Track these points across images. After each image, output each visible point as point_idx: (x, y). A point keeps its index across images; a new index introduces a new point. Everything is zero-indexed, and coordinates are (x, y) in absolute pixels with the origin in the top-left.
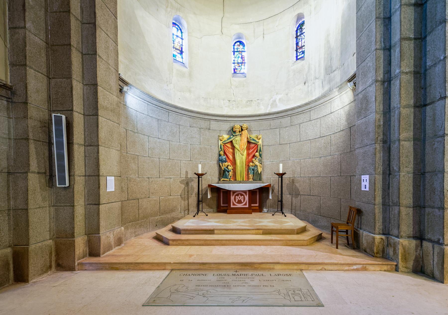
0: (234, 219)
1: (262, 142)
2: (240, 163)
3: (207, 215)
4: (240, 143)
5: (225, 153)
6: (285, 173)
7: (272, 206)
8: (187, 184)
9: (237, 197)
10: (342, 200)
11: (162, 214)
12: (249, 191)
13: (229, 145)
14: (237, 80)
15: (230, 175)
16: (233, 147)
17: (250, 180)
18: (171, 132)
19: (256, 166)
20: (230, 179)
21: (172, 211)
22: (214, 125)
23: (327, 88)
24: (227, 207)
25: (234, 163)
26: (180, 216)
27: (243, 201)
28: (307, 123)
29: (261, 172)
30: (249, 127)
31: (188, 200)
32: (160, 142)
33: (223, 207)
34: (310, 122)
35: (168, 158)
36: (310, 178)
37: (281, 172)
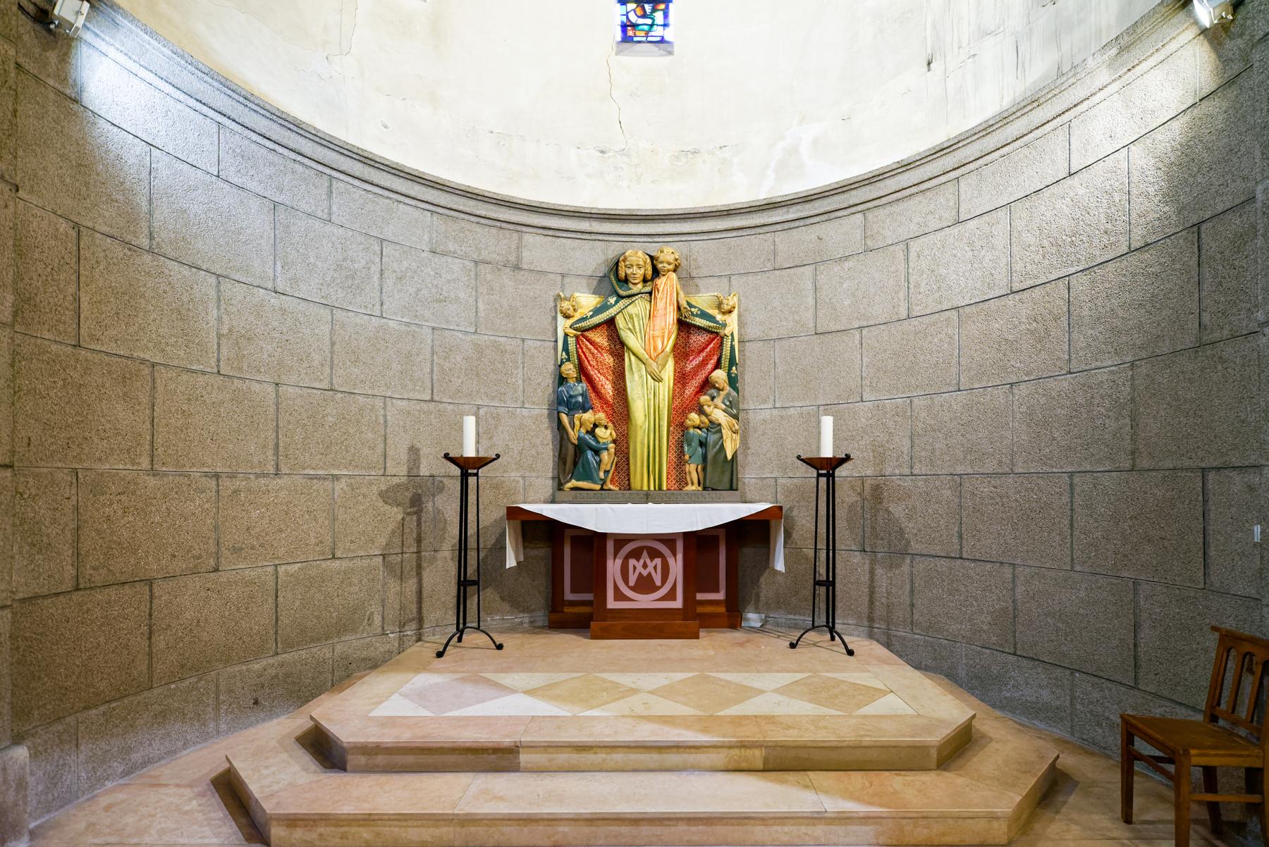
0: (624, 670)
1: (741, 324)
2: (647, 416)
3: (500, 647)
4: (649, 327)
5: (582, 369)
6: (847, 458)
7: (781, 603)
8: (416, 504)
9: (632, 562)
10: (1145, 589)
11: (290, 645)
12: (687, 536)
13: (600, 338)
14: (642, 60)
15: (603, 467)
16: (619, 347)
17: (690, 488)
18: (339, 267)
19: (715, 427)
20: (604, 482)
21: (343, 627)
22: (537, 250)
23: (1039, 69)
24: (589, 603)
25: (621, 412)
26: (381, 647)
27: (658, 583)
28: (940, 235)
29: (735, 456)
30: (684, 263)
31: (419, 575)
32: (283, 311)
33: (572, 604)
34: (960, 227)
35: (325, 385)
36: (958, 480)
37: (827, 452)
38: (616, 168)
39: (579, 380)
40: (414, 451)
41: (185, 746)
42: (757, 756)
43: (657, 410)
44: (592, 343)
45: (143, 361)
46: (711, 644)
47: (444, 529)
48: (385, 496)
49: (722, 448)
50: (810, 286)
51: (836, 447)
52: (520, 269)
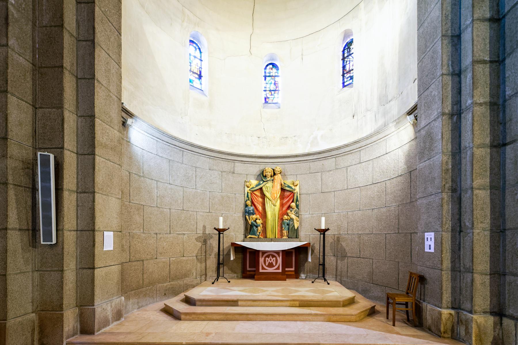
1: (300, 189)
2: (272, 216)
3: (229, 282)
4: (272, 190)
7: (311, 271)
8: (205, 242)
9: (267, 259)
10: (401, 264)
13: (258, 193)
15: (259, 231)
16: (263, 196)
17: (284, 237)
19: (292, 220)
20: (259, 235)
21: (186, 275)
22: (239, 168)
23: (380, 122)
24: (254, 271)
25: (264, 215)
26: (195, 282)
27: (274, 265)
28: (355, 166)
29: (298, 228)
30: (283, 171)
33: (249, 271)
34: (360, 164)
36: (359, 236)
37: (323, 227)
38: (263, 142)
39: (252, 206)
40: (204, 227)
41: (150, 304)
42: (297, 303)
43: (275, 215)
44: (255, 195)
45: (142, 205)
46: (289, 282)
47: (213, 249)
48: (197, 239)
49: (294, 226)
50: (320, 179)
52: (234, 173)
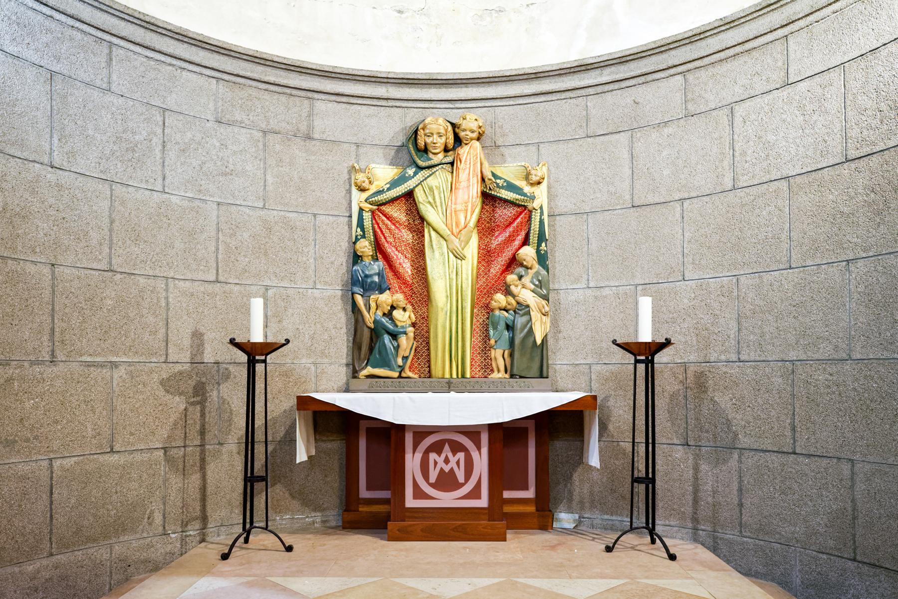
51: (655, 330)
